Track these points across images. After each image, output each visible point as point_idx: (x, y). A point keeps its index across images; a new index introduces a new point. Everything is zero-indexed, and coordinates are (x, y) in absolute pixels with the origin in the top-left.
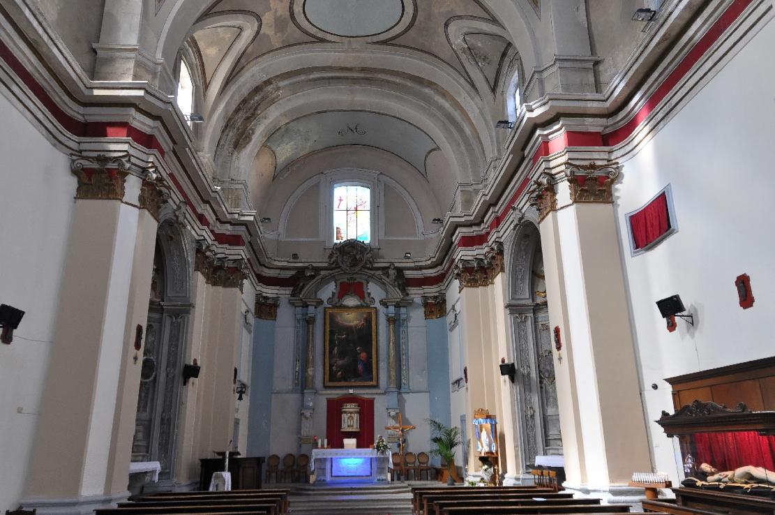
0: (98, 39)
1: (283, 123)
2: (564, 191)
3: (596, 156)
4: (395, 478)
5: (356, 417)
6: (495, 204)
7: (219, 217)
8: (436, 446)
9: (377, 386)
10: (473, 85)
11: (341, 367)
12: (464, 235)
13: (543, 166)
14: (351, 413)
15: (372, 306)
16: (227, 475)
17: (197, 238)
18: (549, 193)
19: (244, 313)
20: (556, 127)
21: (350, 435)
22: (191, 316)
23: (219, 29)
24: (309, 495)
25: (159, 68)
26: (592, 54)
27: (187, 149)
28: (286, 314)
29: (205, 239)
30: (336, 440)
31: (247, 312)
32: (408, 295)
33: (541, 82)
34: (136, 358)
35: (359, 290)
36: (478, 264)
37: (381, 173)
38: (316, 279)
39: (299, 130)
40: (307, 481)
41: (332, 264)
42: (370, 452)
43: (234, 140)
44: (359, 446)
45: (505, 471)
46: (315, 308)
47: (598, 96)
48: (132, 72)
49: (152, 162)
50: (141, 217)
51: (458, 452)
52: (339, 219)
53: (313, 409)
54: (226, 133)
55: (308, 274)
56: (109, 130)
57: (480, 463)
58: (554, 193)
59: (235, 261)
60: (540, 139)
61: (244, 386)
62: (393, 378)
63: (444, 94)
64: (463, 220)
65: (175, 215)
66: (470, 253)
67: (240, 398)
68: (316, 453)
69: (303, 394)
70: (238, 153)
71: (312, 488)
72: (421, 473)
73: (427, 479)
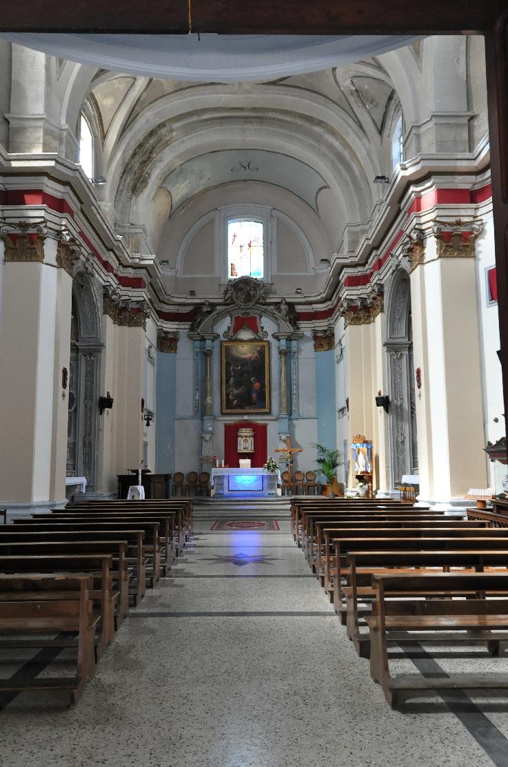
0: (9, 111)
1: (178, 164)
2: (431, 245)
3: (463, 213)
4: (286, 491)
5: (251, 440)
6: (377, 248)
7: (122, 262)
8: (320, 466)
9: (269, 413)
10: (361, 127)
11: (237, 396)
12: (350, 275)
13: (415, 222)
14: (246, 437)
15: (265, 339)
16: (141, 489)
17: (104, 284)
18: (418, 247)
19: (147, 348)
20: (428, 184)
21: (244, 456)
22: (102, 355)
23: (114, 81)
24: (210, 505)
25: (65, 134)
26: (468, 110)
27: (93, 208)
28: (185, 348)
29: (111, 285)
30: (232, 459)
31: (150, 347)
32: (298, 328)
33: (418, 136)
34: (64, 396)
35: (252, 325)
36: (362, 302)
37: (274, 209)
38: (212, 315)
39: (193, 170)
40: (208, 494)
41: (227, 300)
42: (262, 471)
43: (131, 185)
44: (253, 465)
45: (378, 488)
46: (212, 341)
47: (467, 155)
48: (41, 141)
49: (65, 225)
50: (59, 276)
51: (340, 470)
52: (233, 255)
53: (212, 434)
54: (124, 178)
55: (205, 310)
56: (27, 197)
57: (357, 481)
58: (423, 247)
59: (138, 302)
60: (413, 195)
61: (150, 413)
62: (284, 405)
63: (334, 133)
64: (348, 261)
65: (85, 268)
66: (354, 292)
67: (148, 425)
68: (215, 472)
69: (203, 420)
70: (137, 197)
71: (212, 499)
72: (309, 489)
73: (314, 494)
